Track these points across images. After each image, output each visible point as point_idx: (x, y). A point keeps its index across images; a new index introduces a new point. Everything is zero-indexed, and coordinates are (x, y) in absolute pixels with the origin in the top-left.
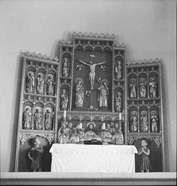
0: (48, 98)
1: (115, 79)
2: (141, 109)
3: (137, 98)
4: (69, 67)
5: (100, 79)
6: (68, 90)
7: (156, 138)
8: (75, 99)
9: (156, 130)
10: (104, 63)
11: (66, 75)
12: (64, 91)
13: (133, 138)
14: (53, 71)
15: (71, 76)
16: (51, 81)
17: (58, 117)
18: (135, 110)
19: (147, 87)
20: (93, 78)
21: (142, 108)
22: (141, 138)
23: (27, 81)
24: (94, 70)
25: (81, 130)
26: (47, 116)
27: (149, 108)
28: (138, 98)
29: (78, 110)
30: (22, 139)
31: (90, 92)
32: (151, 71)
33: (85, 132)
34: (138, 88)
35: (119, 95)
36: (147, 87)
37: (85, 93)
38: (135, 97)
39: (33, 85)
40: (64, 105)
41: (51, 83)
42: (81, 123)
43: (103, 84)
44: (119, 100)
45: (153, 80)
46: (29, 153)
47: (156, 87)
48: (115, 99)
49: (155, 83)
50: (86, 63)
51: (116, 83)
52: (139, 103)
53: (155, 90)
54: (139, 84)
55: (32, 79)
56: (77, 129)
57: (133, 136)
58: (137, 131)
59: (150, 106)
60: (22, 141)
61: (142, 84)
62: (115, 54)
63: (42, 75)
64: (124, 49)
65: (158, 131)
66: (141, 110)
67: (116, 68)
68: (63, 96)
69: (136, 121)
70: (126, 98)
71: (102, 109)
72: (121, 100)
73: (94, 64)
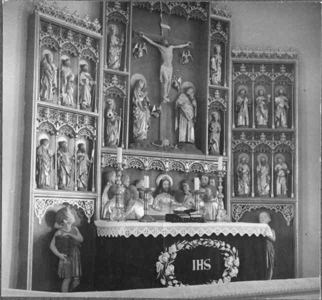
0: (82, 117)
2: (258, 150)
3: (250, 126)
5: (180, 80)
7: (285, 207)
9: (285, 193)
10: (188, 45)
11: (117, 65)
13: (243, 207)
17: (101, 163)
19: (271, 107)
20: (169, 78)
21: (259, 147)
22: (257, 207)
23: (43, 72)
24: (171, 60)
25: (147, 191)
27: (273, 148)
28: (254, 127)
30: (37, 211)
31: (160, 108)
32: (279, 73)
33: (154, 196)
34: (253, 107)
36: (271, 107)
37: (151, 109)
39: (56, 82)
40: (113, 136)
42: (147, 175)
46: (54, 241)
47: (288, 107)
49: (285, 98)
50: (154, 41)
51: (212, 91)
52: (255, 137)
53: (285, 112)
56: (139, 189)
57: (242, 204)
58: (250, 195)
60: (38, 216)
61: (260, 98)
64: (228, 19)
65: (289, 195)
70: (231, 127)
71: (182, 146)
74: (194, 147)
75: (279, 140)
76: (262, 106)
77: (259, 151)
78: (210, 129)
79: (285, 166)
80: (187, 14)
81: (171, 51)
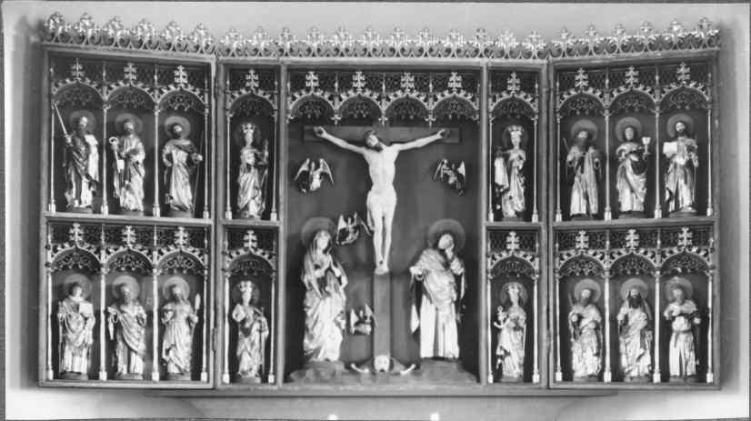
1: (491, 216)
3: (600, 216)
4: (267, 169)
6: (263, 277)
8: (297, 324)
9: (691, 370)
10: (438, 136)
11: (254, 209)
12: (248, 289)
14: (190, 97)
15: (275, 373)
16: (179, 148)
18: (591, 275)
19: (652, 166)
21: (624, 265)
23: (66, 157)
26: (169, 315)
29: (319, 379)
35: (514, 298)
36: (652, 166)
38: (594, 209)
39: (93, 169)
41: (180, 157)
43: (435, 246)
44: (516, 320)
45: (680, 126)
47: (696, 164)
48: (495, 318)
49: (689, 141)
51: (498, 238)
53: (689, 178)
54: (613, 149)
55: (87, 145)
59: (664, 256)
62: (494, 89)
63: (130, 286)
66: (618, 111)
67: (499, 163)
68: (241, 313)
69: (597, 329)
72: (522, 324)
73: (390, 144)
74: (454, 366)
75: (675, 244)
76: (628, 164)
77: (625, 272)
78: (495, 324)
79: (690, 307)
80: (427, 113)
81: (396, 154)
